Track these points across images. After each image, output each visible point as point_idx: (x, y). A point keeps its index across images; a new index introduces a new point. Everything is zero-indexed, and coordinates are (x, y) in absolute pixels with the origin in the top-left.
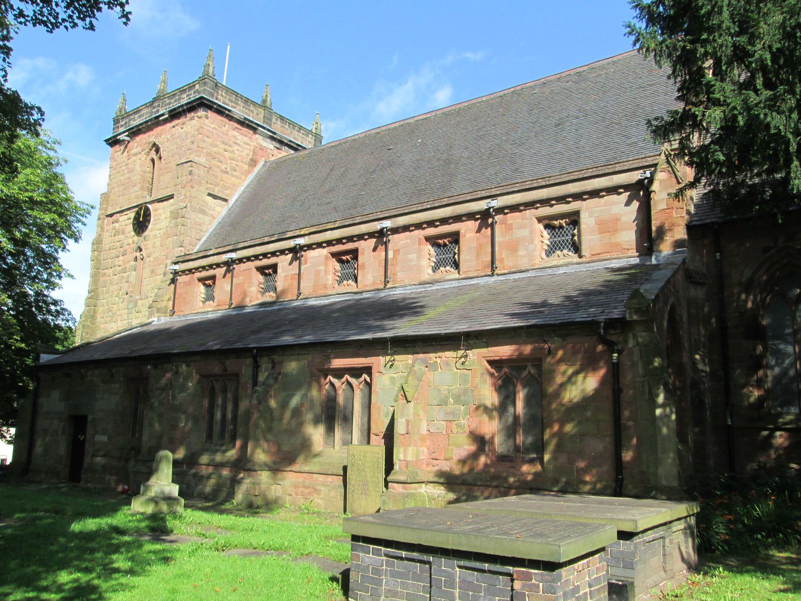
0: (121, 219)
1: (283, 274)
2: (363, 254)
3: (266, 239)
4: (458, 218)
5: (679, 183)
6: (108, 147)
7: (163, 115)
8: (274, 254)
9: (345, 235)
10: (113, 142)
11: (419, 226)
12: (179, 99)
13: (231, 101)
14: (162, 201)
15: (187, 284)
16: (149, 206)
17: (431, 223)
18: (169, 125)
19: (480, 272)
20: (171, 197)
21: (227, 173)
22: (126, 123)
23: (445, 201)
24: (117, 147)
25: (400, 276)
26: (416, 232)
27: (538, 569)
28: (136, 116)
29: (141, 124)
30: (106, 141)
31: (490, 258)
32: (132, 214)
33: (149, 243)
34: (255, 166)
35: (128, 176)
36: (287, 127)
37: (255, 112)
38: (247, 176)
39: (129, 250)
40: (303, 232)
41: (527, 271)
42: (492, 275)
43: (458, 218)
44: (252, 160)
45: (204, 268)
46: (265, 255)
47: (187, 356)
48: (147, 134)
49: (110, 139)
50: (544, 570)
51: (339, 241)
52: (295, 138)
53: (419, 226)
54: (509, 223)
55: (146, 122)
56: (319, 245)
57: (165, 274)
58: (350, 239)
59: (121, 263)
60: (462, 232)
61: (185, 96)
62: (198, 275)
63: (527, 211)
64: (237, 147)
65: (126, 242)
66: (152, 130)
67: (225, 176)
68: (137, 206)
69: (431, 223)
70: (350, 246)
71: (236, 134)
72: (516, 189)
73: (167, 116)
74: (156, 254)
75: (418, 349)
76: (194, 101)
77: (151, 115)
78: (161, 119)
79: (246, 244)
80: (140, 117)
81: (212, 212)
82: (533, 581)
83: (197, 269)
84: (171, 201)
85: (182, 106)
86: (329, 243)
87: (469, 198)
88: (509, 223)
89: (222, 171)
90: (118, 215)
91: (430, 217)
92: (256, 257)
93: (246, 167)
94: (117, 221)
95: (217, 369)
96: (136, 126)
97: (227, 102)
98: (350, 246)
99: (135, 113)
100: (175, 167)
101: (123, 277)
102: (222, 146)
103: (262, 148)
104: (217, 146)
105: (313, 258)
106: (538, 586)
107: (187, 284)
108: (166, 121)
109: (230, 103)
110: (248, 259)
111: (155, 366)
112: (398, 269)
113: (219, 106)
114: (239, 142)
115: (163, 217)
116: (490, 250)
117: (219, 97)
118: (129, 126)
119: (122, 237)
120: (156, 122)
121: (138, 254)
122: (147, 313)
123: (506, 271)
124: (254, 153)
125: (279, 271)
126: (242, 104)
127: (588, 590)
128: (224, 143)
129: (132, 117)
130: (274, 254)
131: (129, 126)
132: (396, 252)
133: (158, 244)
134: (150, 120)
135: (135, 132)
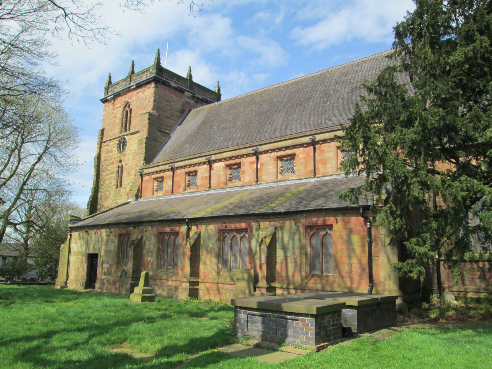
0: (111, 144)
1: (200, 176)
2: (244, 165)
3: (191, 157)
4: (294, 147)
5: (235, 235)
6: (102, 103)
7: (132, 86)
8: (195, 165)
9: (235, 155)
10: (105, 101)
11: (273, 150)
12: (141, 77)
13: (170, 77)
14: (133, 134)
15: (148, 181)
16: (125, 137)
17: (280, 149)
18: (135, 92)
19: (306, 176)
20: (138, 132)
21: (168, 118)
22: (112, 90)
23: (288, 137)
24: (107, 104)
25: (264, 178)
26: (273, 154)
27: (308, 317)
28: (117, 86)
29: (121, 91)
30: (101, 100)
31: (313, 168)
32: (116, 142)
33: (126, 158)
34: (184, 113)
35: (113, 120)
36: (201, 90)
37: (183, 82)
38: (179, 119)
39: (115, 162)
40: (211, 153)
41: (332, 175)
42: (315, 177)
43: (294, 147)
44: (182, 110)
45: (157, 172)
46: (190, 166)
47: (151, 223)
48: (124, 97)
49: (103, 99)
50: (311, 317)
51: (231, 158)
52: (205, 96)
53: (273, 150)
54: (322, 149)
55: (123, 90)
56: (220, 160)
57: (135, 175)
58: (236, 157)
59: (110, 169)
60: (297, 154)
61: (145, 75)
62: (154, 176)
63: (332, 143)
64: (174, 103)
65: (113, 157)
66: (126, 94)
67: (167, 119)
68: (119, 137)
69: (280, 149)
70: (237, 161)
71: (173, 96)
72: (325, 131)
73: (135, 87)
74: (130, 164)
75: (271, 219)
76: (150, 78)
77: (126, 86)
78: (131, 88)
79: (180, 159)
80: (119, 87)
81: (160, 140)
82: (307, 322)
83: (153, 173)
84: (138, 134)
85: (143, 81)
86: (225, 159)
87: (300, 135)
88: (322, 149)
89: (166, 117)
90: (109, 142)
91: (279, 145)
92: (186, 166)
93: (178, 114)
94: (108, 145)
95: (168, 229)
96: (118, 92)
97: (168, 78)
98: (237, 161)
99: (117, 84)
100: (139, 115)
101: (112, 177)
102: (166, 103)
103: (188, 103)
104: (162, 103)
105: (217, 167)
106: (308, 324)
107: (148, 181)
108: (134, 89)
109: (169, 78)
110: (181, 167)
111: (134, 228)
112: (263, 174)
113: (163, 80)
114: (174, 100)
115: (133, 143)
116: (313, 164)
117: (163, 75)
118: (114, 92)
119: (110, 154)
120: (128, 90)
121: (120, 164)
122: (126, 197)
123: (321, 175)
124: (183, 106)
125: (198, 174)
126: (176, 79)
127: (332, 328)
128: (166, 101)
129: (115, 87)
130: (195, 165)
131: (114, 92)
132: (262, 165)
133: (131, 158)
134: (126, 89)
135: (117, 95)
